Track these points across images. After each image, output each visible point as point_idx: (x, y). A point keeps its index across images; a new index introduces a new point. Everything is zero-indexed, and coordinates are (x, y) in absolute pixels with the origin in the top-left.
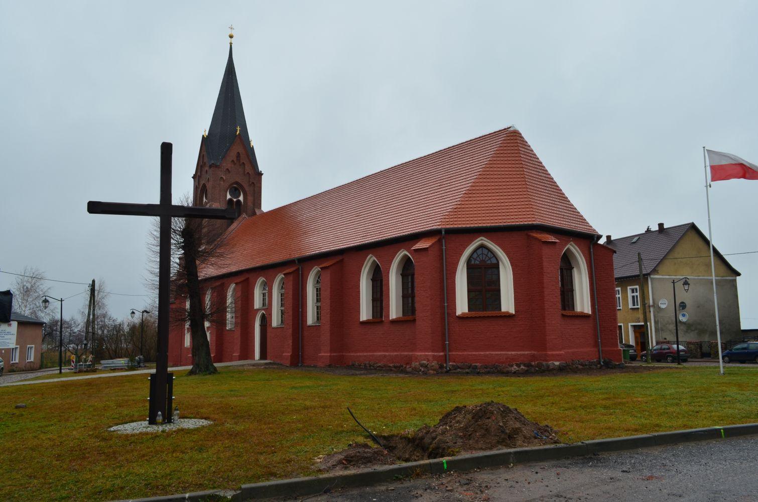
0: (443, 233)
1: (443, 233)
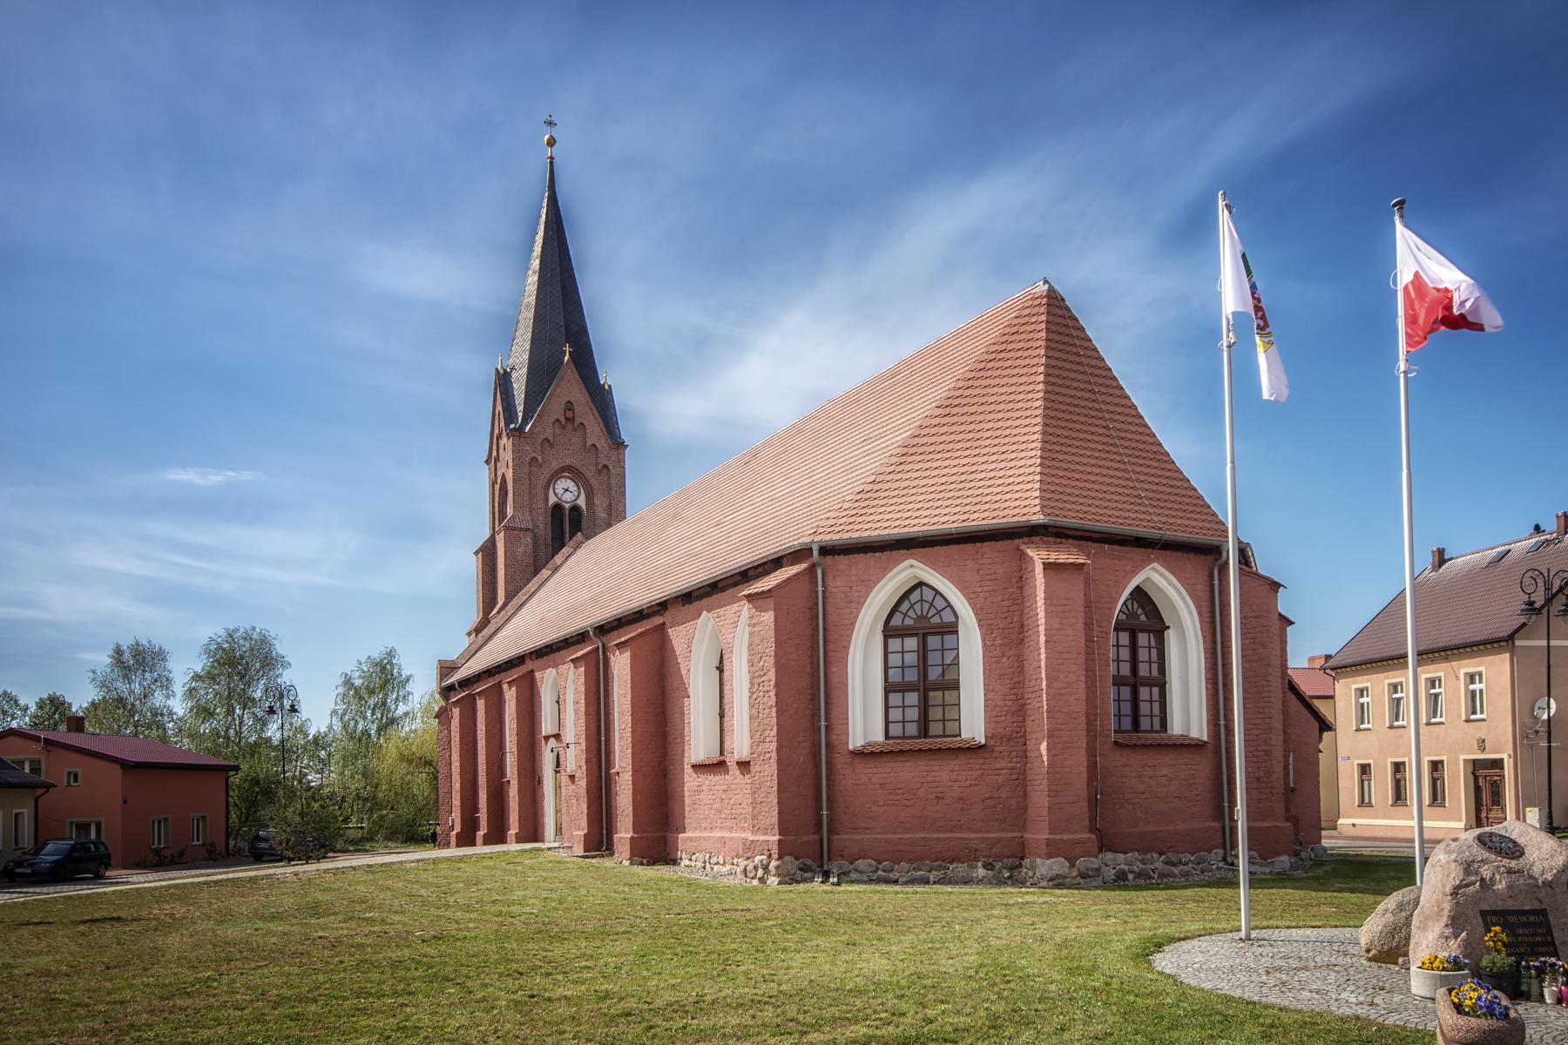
0: (815, 553)
1: (815, 553)
